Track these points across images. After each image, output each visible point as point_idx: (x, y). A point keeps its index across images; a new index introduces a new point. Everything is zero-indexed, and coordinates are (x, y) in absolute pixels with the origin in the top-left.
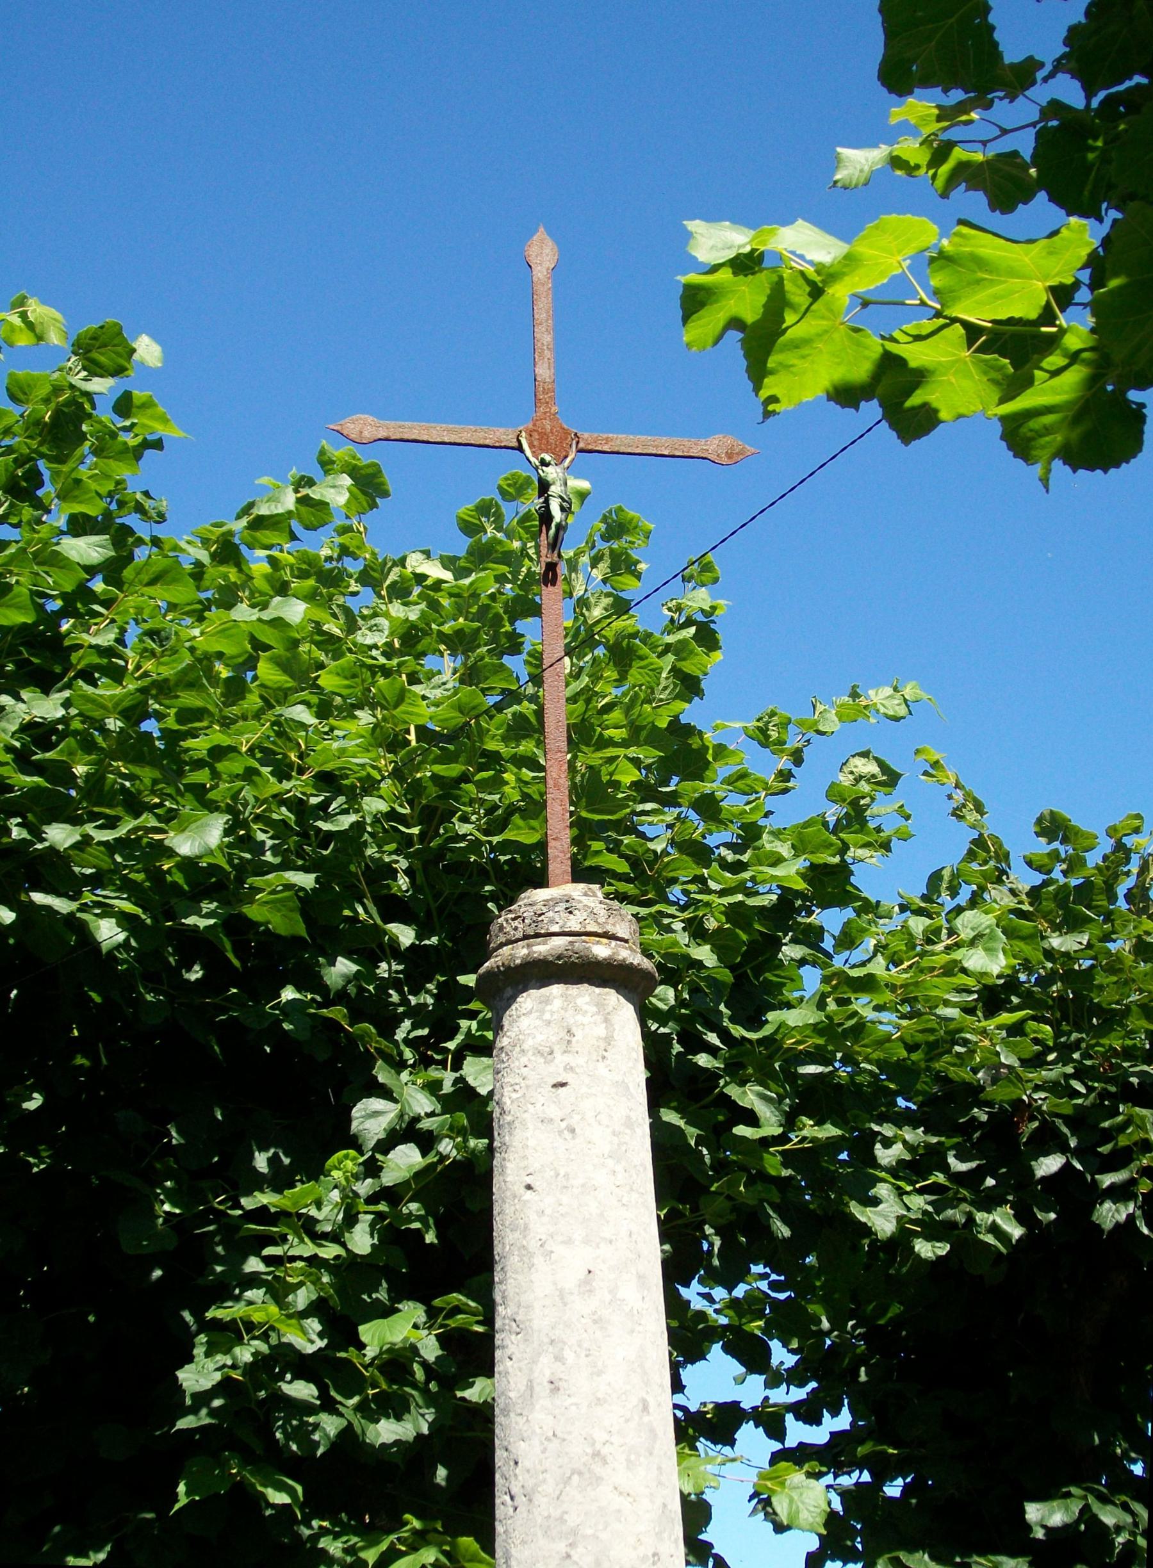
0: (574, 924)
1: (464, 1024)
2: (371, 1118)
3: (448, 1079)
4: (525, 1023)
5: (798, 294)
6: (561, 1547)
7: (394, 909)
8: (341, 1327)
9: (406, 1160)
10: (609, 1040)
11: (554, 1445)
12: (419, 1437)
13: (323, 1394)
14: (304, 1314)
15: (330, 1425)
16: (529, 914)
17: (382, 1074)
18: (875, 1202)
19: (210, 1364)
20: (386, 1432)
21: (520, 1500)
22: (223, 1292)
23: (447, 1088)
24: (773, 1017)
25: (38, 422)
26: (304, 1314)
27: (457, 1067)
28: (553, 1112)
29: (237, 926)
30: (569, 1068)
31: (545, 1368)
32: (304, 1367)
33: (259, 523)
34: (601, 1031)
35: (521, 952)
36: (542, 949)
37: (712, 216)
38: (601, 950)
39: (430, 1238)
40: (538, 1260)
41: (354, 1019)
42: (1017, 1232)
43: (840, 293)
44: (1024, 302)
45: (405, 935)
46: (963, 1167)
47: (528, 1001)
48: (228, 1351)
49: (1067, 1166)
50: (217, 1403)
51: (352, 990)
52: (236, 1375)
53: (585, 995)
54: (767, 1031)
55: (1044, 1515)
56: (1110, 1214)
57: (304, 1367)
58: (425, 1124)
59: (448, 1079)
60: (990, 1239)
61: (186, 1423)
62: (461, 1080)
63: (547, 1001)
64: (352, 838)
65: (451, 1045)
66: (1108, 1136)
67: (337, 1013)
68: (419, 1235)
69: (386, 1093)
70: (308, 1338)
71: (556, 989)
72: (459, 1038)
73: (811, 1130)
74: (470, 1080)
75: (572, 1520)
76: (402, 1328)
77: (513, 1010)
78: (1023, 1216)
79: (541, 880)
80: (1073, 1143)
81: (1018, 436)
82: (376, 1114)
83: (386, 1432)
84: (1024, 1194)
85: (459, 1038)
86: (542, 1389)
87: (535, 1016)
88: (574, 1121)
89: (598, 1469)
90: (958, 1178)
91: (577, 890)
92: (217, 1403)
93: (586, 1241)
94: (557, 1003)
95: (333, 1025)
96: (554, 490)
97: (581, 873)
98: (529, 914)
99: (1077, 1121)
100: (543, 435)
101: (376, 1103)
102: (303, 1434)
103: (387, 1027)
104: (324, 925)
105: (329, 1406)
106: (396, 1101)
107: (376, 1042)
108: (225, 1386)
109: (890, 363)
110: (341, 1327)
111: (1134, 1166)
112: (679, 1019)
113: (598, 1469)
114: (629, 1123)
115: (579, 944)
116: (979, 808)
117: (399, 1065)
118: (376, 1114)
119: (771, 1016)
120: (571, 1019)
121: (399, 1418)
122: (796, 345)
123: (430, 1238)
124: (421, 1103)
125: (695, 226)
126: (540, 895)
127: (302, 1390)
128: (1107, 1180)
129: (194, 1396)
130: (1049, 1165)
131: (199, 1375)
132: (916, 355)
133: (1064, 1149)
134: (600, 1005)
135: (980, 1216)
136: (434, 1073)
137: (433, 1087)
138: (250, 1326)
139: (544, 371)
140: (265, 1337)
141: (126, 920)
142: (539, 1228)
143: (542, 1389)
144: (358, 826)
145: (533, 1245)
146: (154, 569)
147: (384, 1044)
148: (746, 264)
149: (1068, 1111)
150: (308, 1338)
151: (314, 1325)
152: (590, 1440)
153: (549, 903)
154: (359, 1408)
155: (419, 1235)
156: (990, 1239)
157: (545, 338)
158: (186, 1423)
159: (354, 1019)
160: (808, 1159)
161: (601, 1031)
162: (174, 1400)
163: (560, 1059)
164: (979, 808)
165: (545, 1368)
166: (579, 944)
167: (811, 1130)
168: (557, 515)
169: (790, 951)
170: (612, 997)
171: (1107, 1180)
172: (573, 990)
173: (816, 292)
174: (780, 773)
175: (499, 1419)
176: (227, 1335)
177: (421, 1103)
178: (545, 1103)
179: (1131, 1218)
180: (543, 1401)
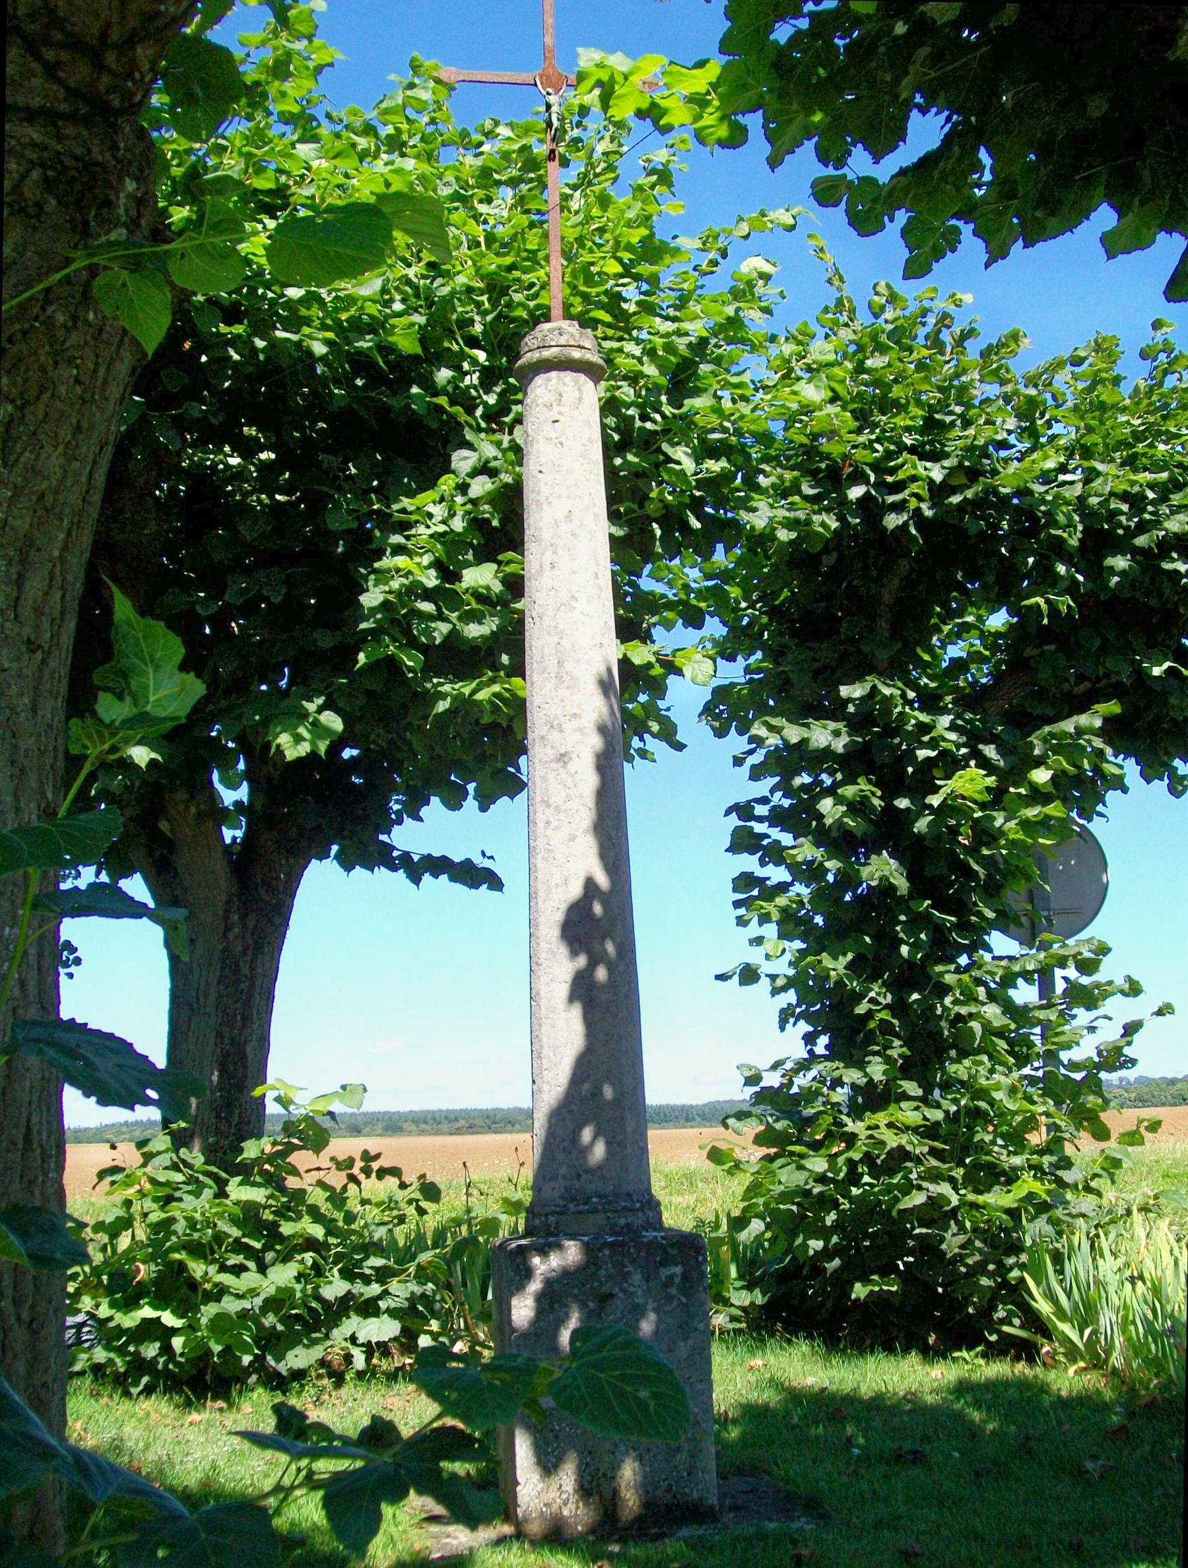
0: (563, 341)
1: (514, 407)
2: (463, 461)
3: (506, 439)
4: (538, 391)
5: (619, 79)
6: (556, 639)
7: (473, 342)
8: (449, 573)
9: (481, 486)
10: (580, 399)
11: (552, 593)
12: (493, 632)
13: (439, 609)
14: (427, 568)
15: (444, 628)
16: (540, 336)
17: (469, 435)
18: (754, 510)
19: (377, 590)
20: (474, 631)
21: (537, 619)
22: (379, 554)
23: (505, 445)
24: (688, 403)
25: (266, 66)
26: (427, 568)
27: (511, 433)
28: (552, 435)
29: (385, 349)
30: (560, 413)
31: (548, 557)
32: (428, 594)
33: (386, 112)
34: (577, 394)
35: (536, 356)
36: (546, 354)
37: (587, 45)
38: (576, 354)
39: (495, 523)
40: (545, 506)
41: (452, 403)
42: (834, 525)
43: (635, 79)
44: (702, 87)
45: (481, 356)
46: (811, 492)
47: (540, 380)
48: (386, 584)
49: (868, 492)
50: (379, 616)
51: (450, 388)
52: (391, 597)
53: (569, 377)
54: (684, 410)
55: (852, 691)
56: (892, 521)
57: (428, 594)
58: (493, 464)
59: (506, 439)
60: (821, 530)
61: (363, 626)
62: (512, 441)
63: (549, 380)
64: (448, 301)
65: (507, 419)
66: (893, 471)
67: (443, 401)
68: (488, 521)
69: (470, 446)
70: (431, 580)
71: (554, 374)
72: (511, 416)
73: (714, 466)
74: (518, 441)
75: (561, 627)
76: (480, 576)
77: (532, 385)
78: (841, 518)
79: (548, 320)
80: (872, 479)
81: (700, 137)
82: (465, 458)
83: (474, 631)
84: (841, 507)
85: (511, 416)
86: (547, 566)
87: (543, 388)
88: (563, 439)
89: (573, 604)
90: (806, 498)
91: (565, 324)
92: (379, 616)
93: (569, 497)
94: (554, 381)
95: (439, 409)
96: (555, 109)
97: (568, 316)
98: (540, 336)
99: (875, 467)
100: (548, 77)
101: (465, 453)
102: (428, 632)
103: (470, 411)
104: (433, 355)
105: (440, 617)
106: (475, 450)
107: (463, 417)
108: (385, 605)
109: (654, 105)
110: (449, 573)
111: (907, 492)
112: (638, 406)
113: (573, 604)
114: (590, 440)
115: (566, 351)
116: (841, 279)
117: (479, 429)
118: (465, 458)
119: (686, 402)
120: (562, 388)
121: (480, 623)
122: (620, 97)
123: (495, 523)
124: (490, 451)
125: (580, 50)
126: (546, 326)
127: (427, 607)
128: (890, 499)
129: (370, 609)
130: (856, 493)
131: (371, 598)
132: (664, 103)
133: (867, 483)
134: (576, 382)
135: (815, 518)
136: (497, 436)
137: (498, 444)
138: (398, 570)
139: (549, 40)
140: (406, 576)
141: (328, 342)
142: (545, 491)
143: (547, 566)
144: (453, 293)
145: (542, 499)
146: (336, 150)
147: (469, 419)
148: (601, 66)
149: (869, 460)
150: (431, 580)
151: (433, 573)
152: (570, 590)
153: (551, 331)
154: (460, 618)
155: (488, 521)
156: (821, 530)
157: (549, 21)
158: (363, 626)
159: (452, 403)
160: (712, 484)
161: (577, 394)
162: (359, 613)
163: (556, 408)
164: (841, 279)
165: (548, 557)
166: (566, 351)
167: (714, 466)
168: (556, 123)
169: (705, 368)
170: (582, 378)
171: (890, 499)
172: (562, 374)
173: (626, 78)
174: (711, 261)
175: (527, 583)
176: (383, 576)
177: (490, 451)
178: (548, 430)
179: (906, 524)
180: (547, 572)
